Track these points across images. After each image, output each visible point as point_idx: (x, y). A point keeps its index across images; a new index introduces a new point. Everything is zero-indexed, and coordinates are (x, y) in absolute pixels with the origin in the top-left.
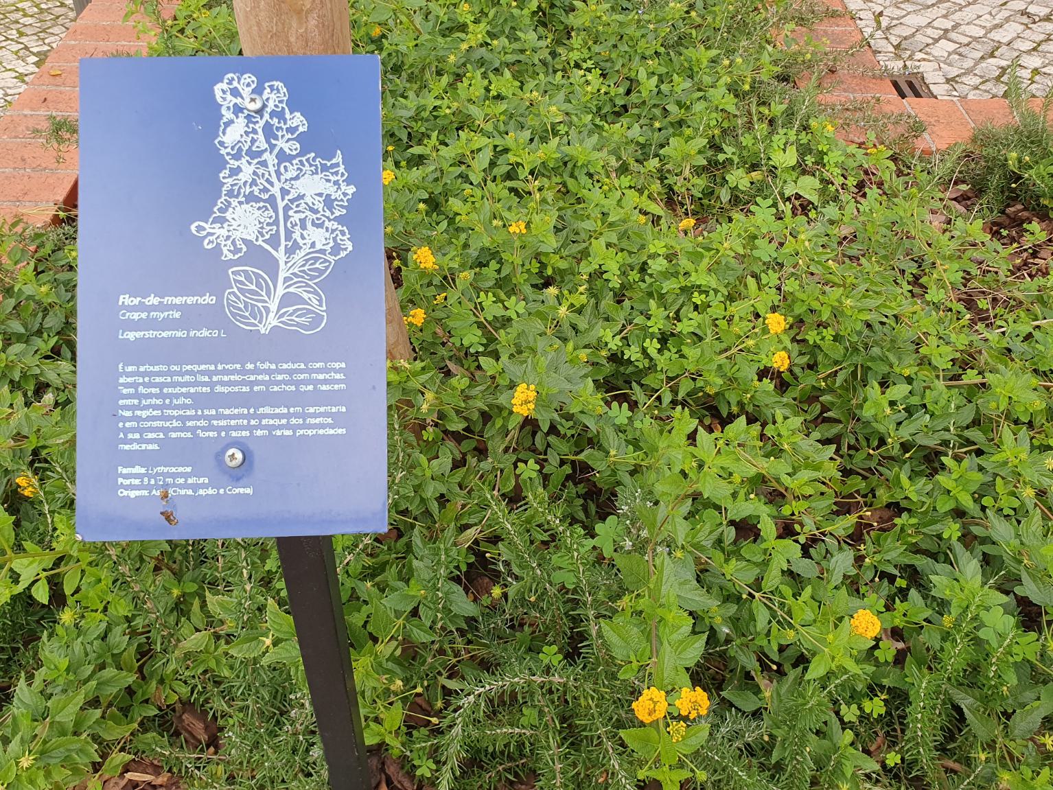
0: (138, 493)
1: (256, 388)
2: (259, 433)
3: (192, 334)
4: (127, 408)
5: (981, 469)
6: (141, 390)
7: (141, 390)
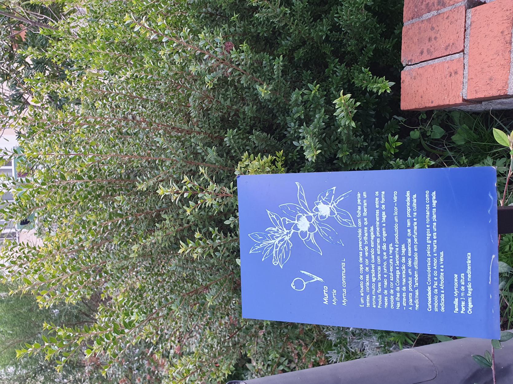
1: (409, 231)
4: (395, 305)
6: (379, 291)
7: (379, 291)
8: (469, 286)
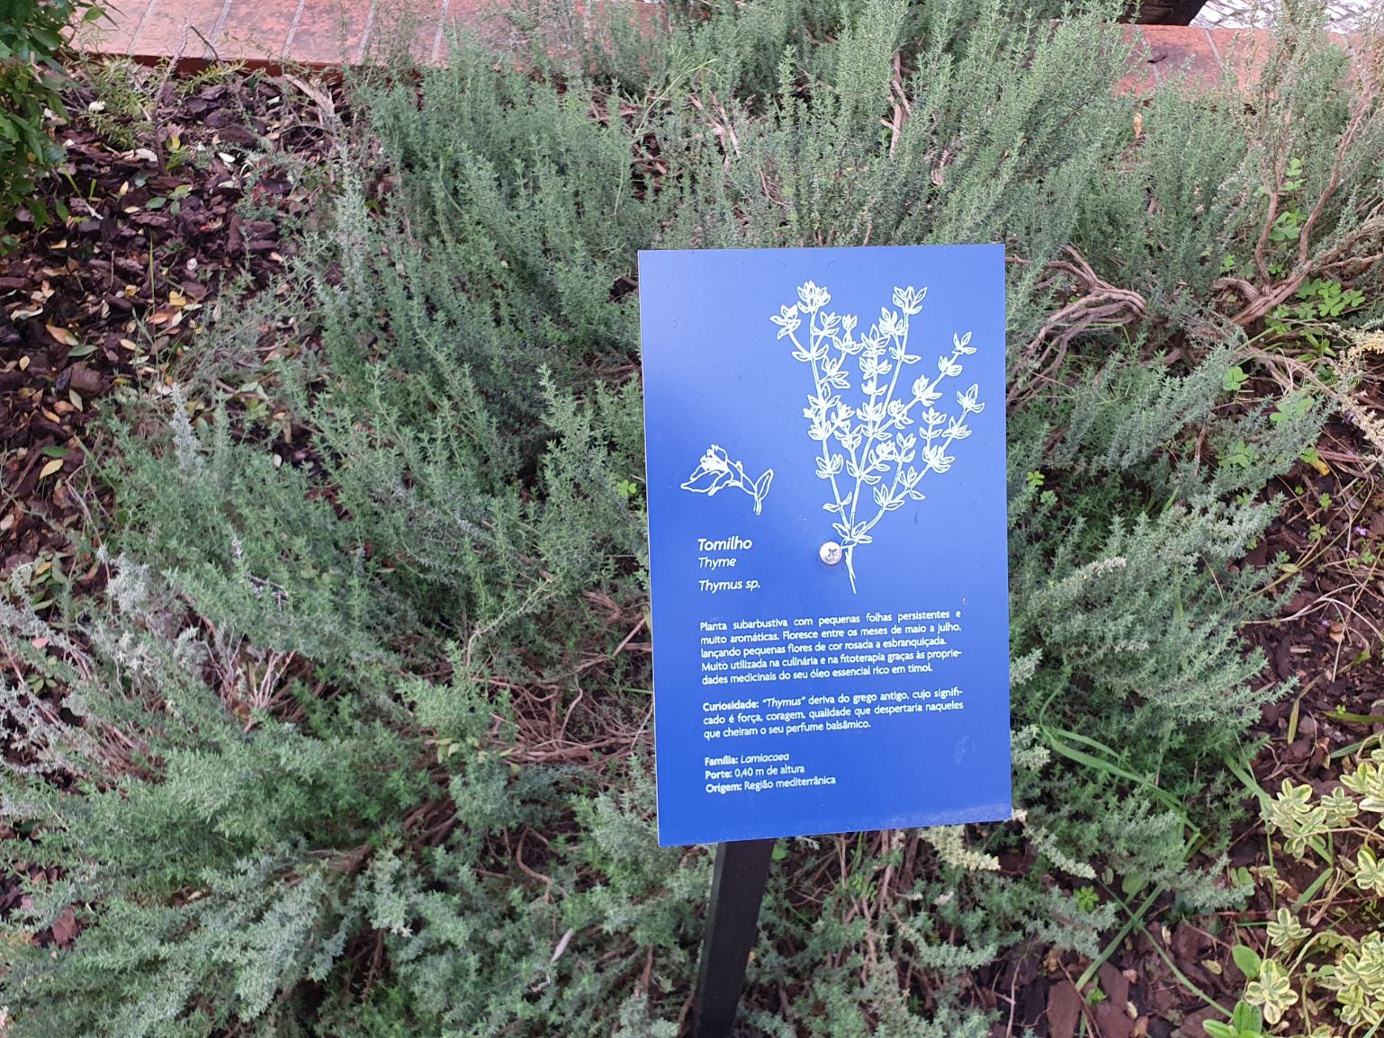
0: (728, 788)
2: (924, 695)
3: (739, 585)
5: (30, 921)
8: (766, 785)
